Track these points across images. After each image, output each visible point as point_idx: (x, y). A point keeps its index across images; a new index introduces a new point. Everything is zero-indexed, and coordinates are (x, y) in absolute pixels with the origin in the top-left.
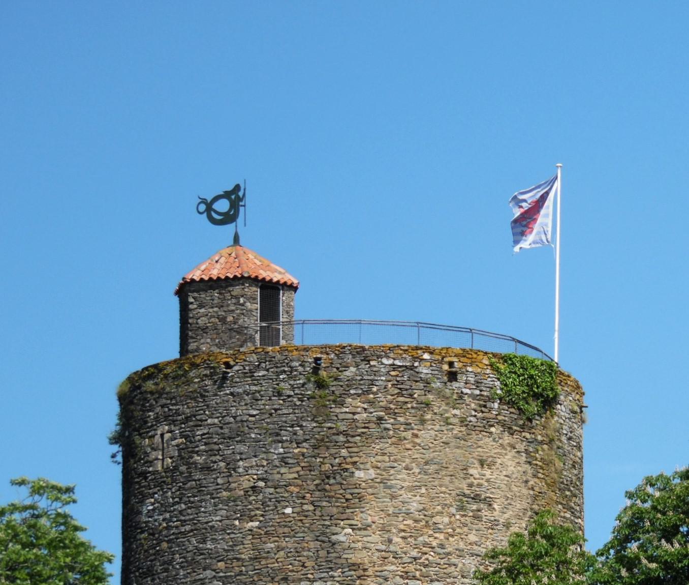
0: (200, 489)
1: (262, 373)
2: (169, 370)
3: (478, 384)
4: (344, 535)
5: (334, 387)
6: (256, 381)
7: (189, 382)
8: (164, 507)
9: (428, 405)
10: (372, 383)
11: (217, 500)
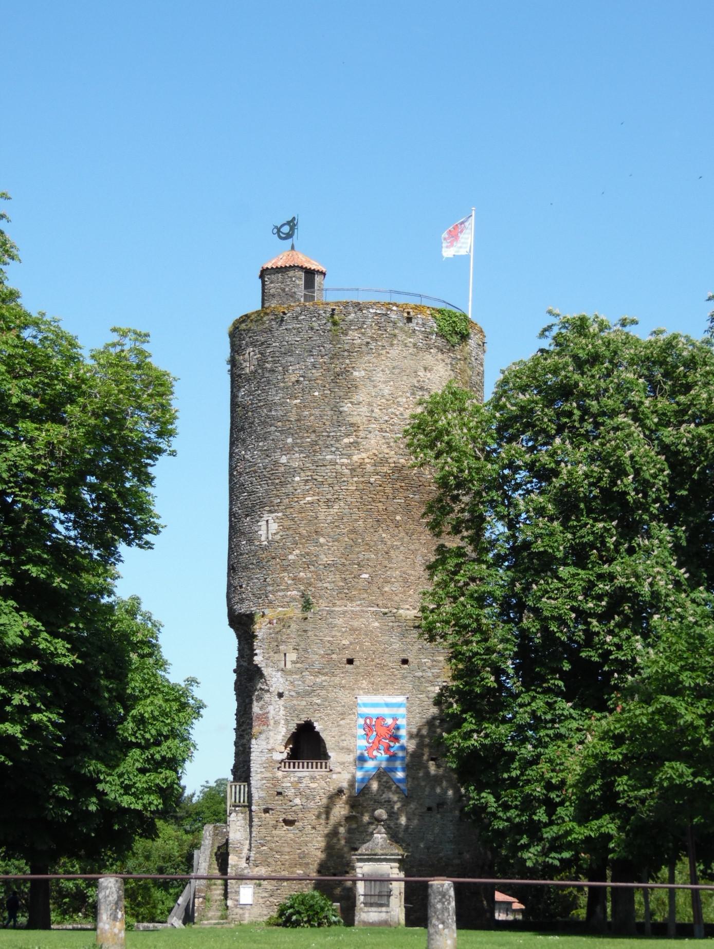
0: (269, 382)
2: (253, 317)
3: (424, 325)
4: (347, 407)
5: (343, 325)
6: (300, 322)
7: (263, 323)
8: (250, 393)
9: (395, 335)
10: (364, 323)
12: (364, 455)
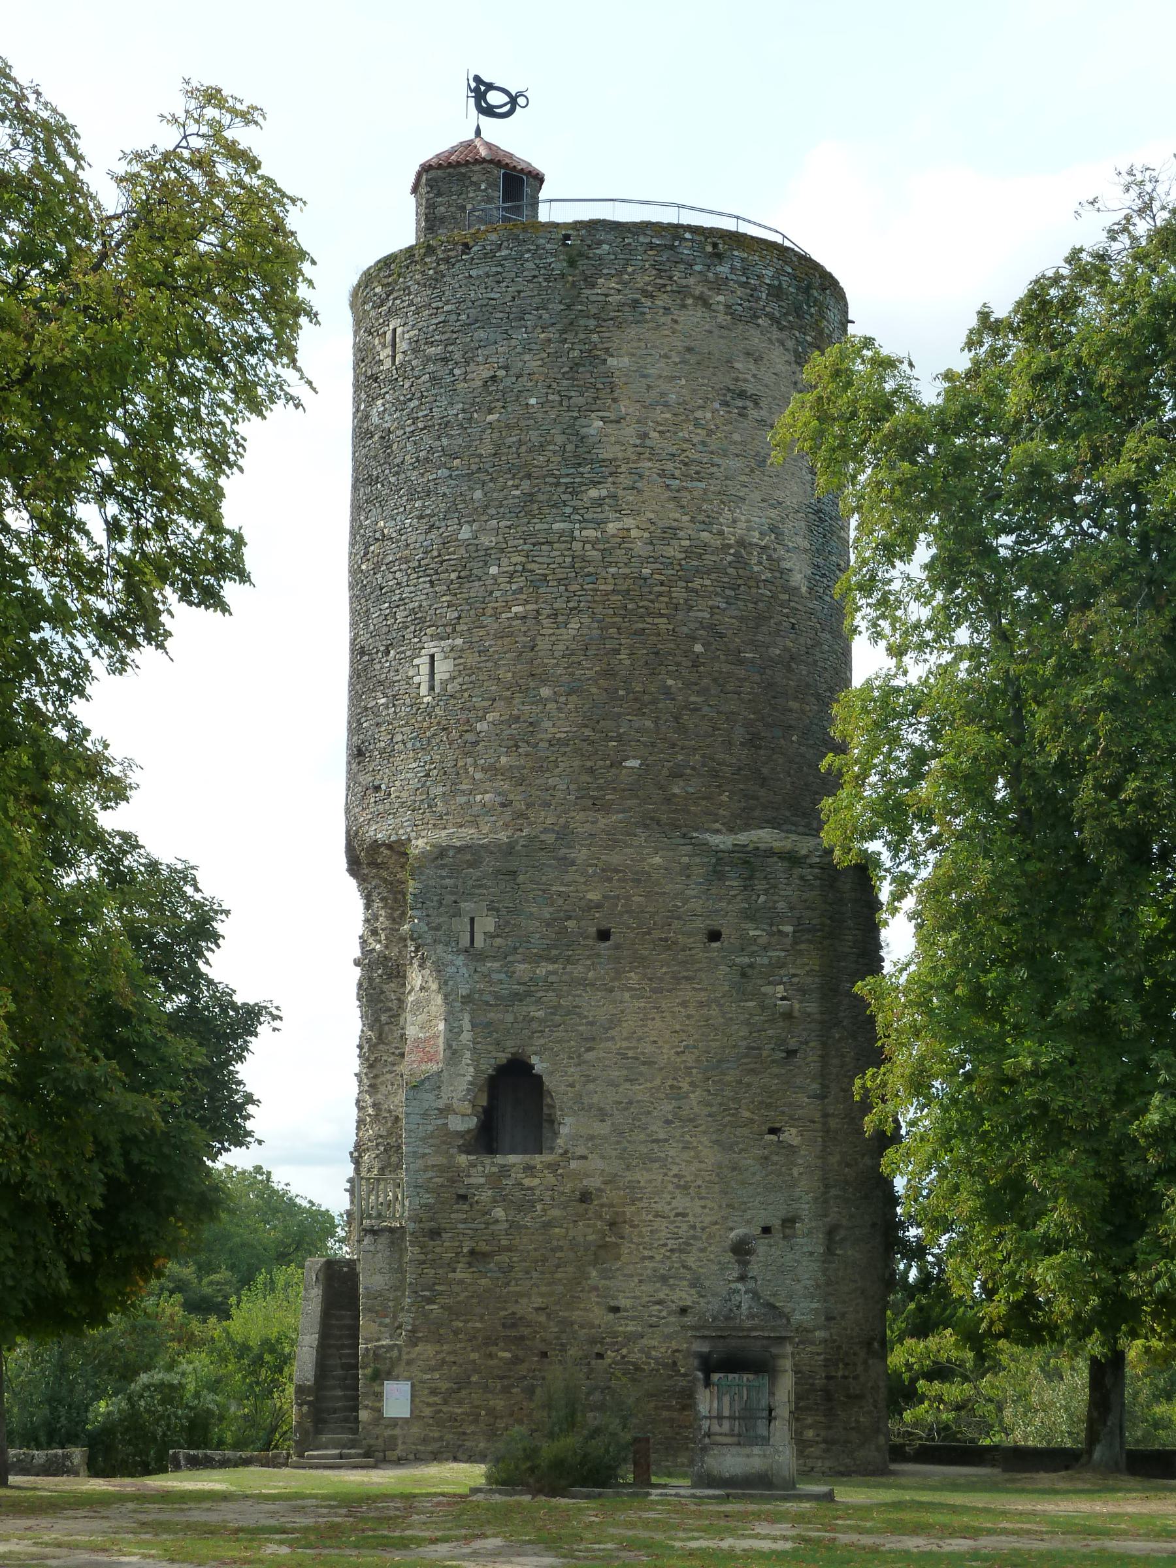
1: (504, 253)
11: (46, 1538)
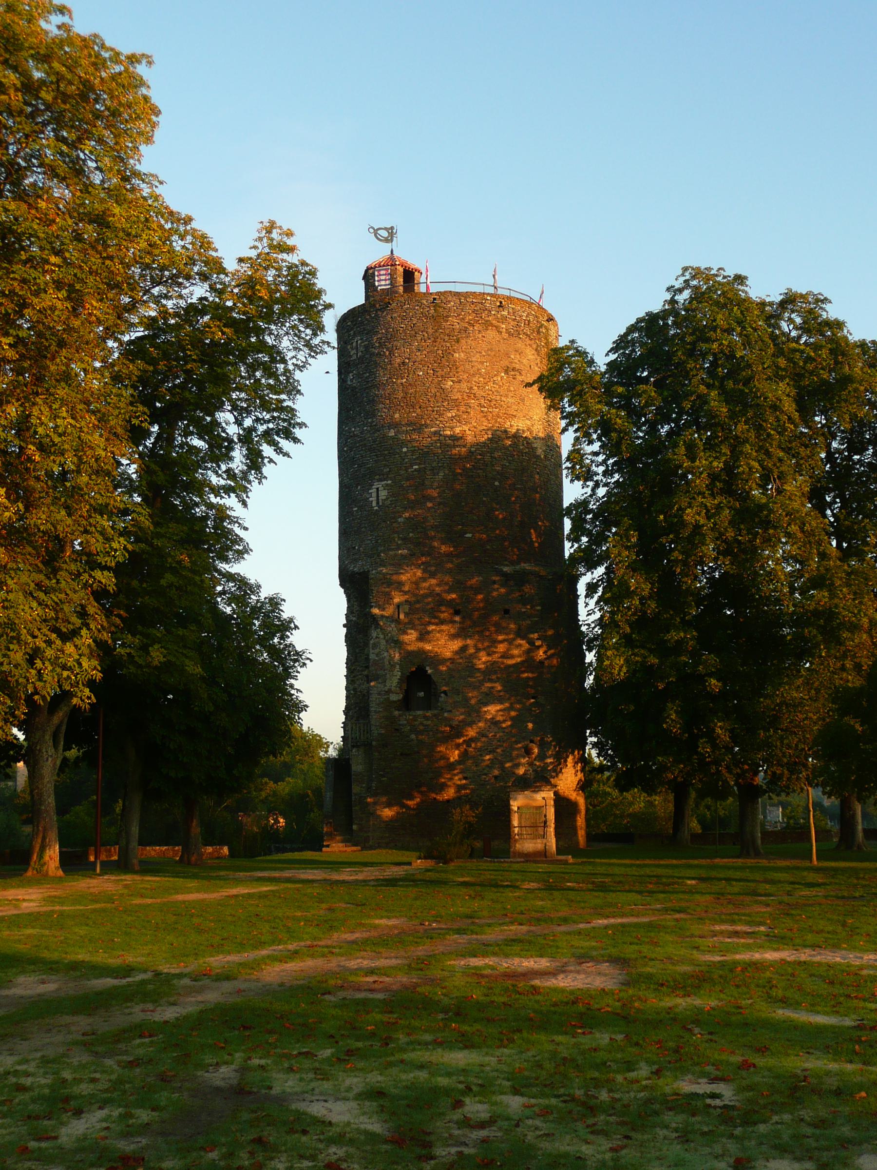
12: (466, 428)
